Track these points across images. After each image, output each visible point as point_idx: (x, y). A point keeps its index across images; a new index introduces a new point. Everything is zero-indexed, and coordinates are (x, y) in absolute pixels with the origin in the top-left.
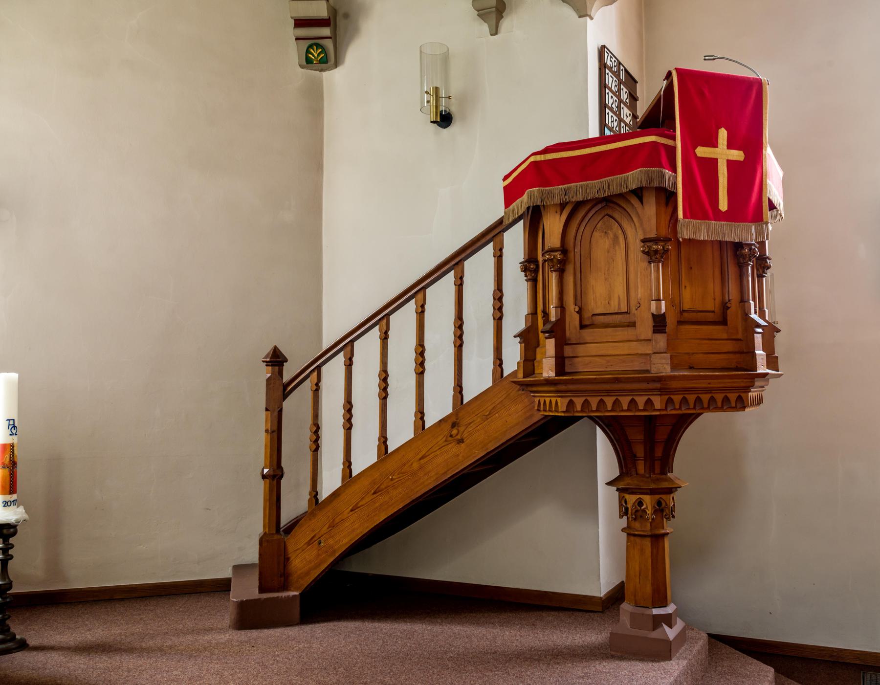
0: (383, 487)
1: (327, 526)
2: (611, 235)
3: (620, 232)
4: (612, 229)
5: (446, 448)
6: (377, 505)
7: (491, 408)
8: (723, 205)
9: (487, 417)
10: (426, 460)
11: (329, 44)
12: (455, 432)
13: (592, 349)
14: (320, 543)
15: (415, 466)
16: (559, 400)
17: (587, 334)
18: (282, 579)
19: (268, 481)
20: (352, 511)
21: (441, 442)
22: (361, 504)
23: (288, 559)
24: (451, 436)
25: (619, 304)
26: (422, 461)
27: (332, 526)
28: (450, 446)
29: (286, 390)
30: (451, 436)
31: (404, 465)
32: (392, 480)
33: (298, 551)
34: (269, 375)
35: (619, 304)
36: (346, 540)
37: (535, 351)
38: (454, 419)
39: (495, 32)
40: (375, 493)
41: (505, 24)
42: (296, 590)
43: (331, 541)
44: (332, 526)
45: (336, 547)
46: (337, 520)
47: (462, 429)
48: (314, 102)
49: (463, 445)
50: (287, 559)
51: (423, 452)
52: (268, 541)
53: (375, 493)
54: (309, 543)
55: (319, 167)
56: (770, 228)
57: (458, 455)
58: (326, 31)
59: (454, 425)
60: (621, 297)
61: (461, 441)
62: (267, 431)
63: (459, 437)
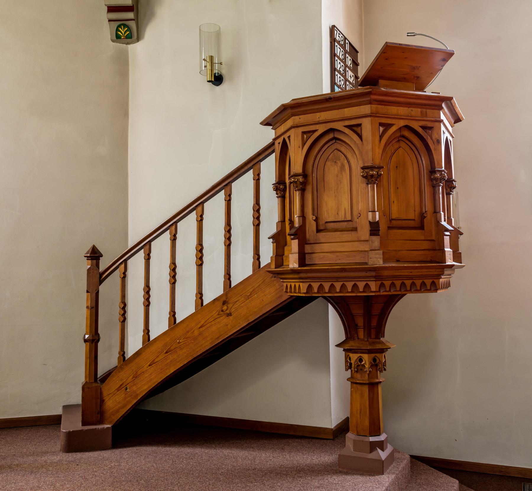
0: (172, 348)
1: (132, 376)
2: (339, 164)
3: (346, 161)
4: (340, 160)
5: (219, 320)
6: (168, 361)
7: (251, 290)
9: (248, 297)
10: (203, 328)
11: (133, 24)
12: (225, 308)
13: (326, 247)
14: (126, 389)
15: (196, 333)
18: (99, 416)
20: (150, 365)
22: (155, 361)
23: (103, 401)
24: (222, 311)
25: (345, 215)
27: (136, 377)
28: (222, 318)
29: (101, 278)
30: (222, 311)
31: (188, 332)
32: (179, 343)
35: (345, 215)
40: (166, 353)
42: (109, 423)
43: (134, 388)
44: (136, 377)
45: (138, 392)
46: (139, 372)
47: (230, 306)
49: (231, 317)
50: (102, 401)
51: (202, 323)
53: (166, 353)
54: (118, 389)
55: (125, 114)
57: (227, 325)
58: (130, 15)
59: (224, 303)
60: (347, 209)
61: (229, 315)
62: (87, 307)
63: (228, 312)
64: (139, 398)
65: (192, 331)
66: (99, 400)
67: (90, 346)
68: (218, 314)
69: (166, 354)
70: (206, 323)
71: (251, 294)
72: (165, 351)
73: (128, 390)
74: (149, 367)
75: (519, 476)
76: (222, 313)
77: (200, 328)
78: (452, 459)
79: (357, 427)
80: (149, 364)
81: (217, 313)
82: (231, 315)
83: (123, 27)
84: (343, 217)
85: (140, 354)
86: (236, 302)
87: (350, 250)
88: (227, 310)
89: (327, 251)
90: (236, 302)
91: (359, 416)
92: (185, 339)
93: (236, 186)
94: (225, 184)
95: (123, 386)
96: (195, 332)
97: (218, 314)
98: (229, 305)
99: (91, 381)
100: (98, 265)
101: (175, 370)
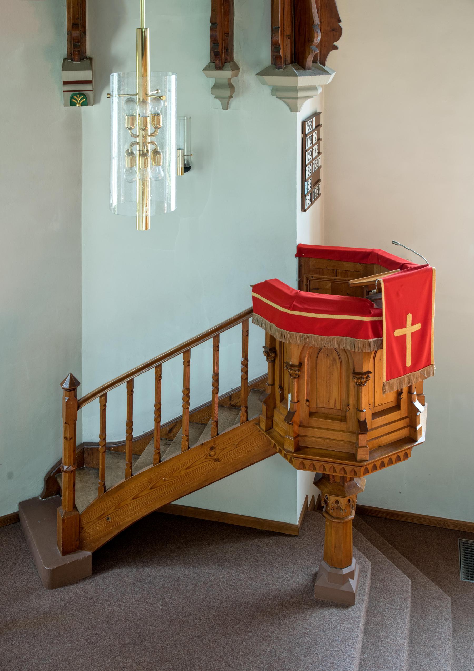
0: (158, 485)
1: (114, 508)
2: (331, 358)
3: (337, 357)
4: (331, 354)
5: (206, 463)
6: (154, 497)
7: (239, 440)
8: (409, 363)
9: (236, 447)
10: (190, 470)
11: (90, 93)
12: (212, 453)
13: (318, 433)
14: (108, 519)
15: (183, 473)
16: (296, 461)
17: (314, 421)
18: (78, 542)
19: (67, 474)
20: (133, 499)
21: (202, 459)
22: (140, 495)
23: (83, 528)
24: (210, 456)
25: (335, 404)
26: (188, 470)
27: (118, 508)
28: (209, 462)
29: (80, 404)
30: (210, 456)
31: (174, 471)
32: (165, 481)
33: (90, 524)
34: (67, 399)
35: (335, 404)
36: (129, 519)
37: (273, 411)
38: (212, 444)
39: (226, 107)
40: (151, 488)
41: (234, 103)
42: (89, 550)
43: (117, 519)
44: (118, 508)
45: (121, 523)
46: (122, 504)
47: (217, 452)
48: (75, 130)
49: (218, 463)
50: (81, 528)
51: (189, 464)
52: (68, 518)
53: (151, 488)
54: (99, 518)
55: (79, 182)
56: (435, 368)
57: (215, 470)
58: (89, 87)
59: (212, 448)
60: (337, 399)
61: (217, 460)
62: (66, 438)
63: (216, 457)
64: (122, 529)
65: (179, 471)
66: (78, 528)
67: (69, 476)
68: (206, 459)
69: (152, 490)
70: (193, 465)
71: (238, 444)
72: (150, 487)
73: (110, 520)
74: (133, 500)
75: (456, 529)
76: (209, 457)
77: (186, 469)
78: (396, 510)
79: (331, 560)
80: (133, 497)
81: (205, 457)
82: (219, 461)
83: (78, 96)
84: (334, 406)
85: (124, 487)
86: (224, 449)
87: (340, 439)
88: (214, 455)
89: (318, 436)
90: (224, 449)
91: (333, 550)
92: (172, 478)
93: (223, 336)
94: (214, 334)
95: (104, 516)
96: (182, 472)
97: (206, 459)
98: (216, 451)
99: (70, 510)
100: (75, 396)
101: (160, 506)
